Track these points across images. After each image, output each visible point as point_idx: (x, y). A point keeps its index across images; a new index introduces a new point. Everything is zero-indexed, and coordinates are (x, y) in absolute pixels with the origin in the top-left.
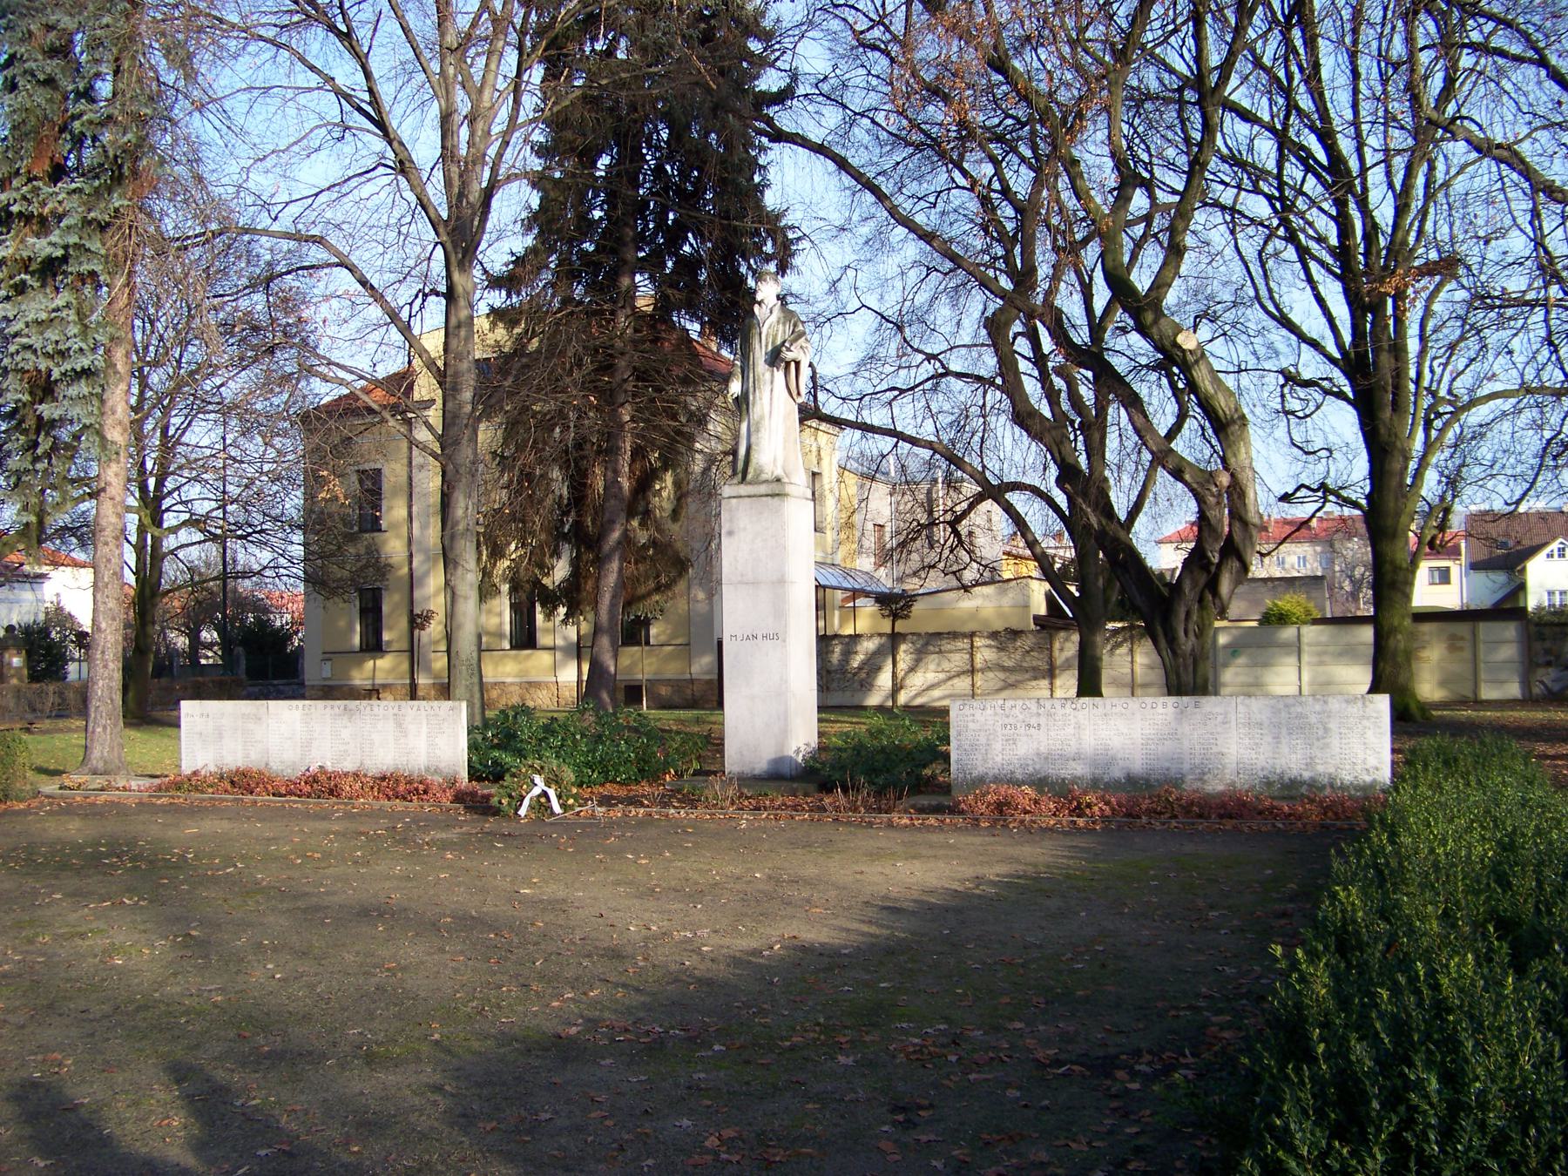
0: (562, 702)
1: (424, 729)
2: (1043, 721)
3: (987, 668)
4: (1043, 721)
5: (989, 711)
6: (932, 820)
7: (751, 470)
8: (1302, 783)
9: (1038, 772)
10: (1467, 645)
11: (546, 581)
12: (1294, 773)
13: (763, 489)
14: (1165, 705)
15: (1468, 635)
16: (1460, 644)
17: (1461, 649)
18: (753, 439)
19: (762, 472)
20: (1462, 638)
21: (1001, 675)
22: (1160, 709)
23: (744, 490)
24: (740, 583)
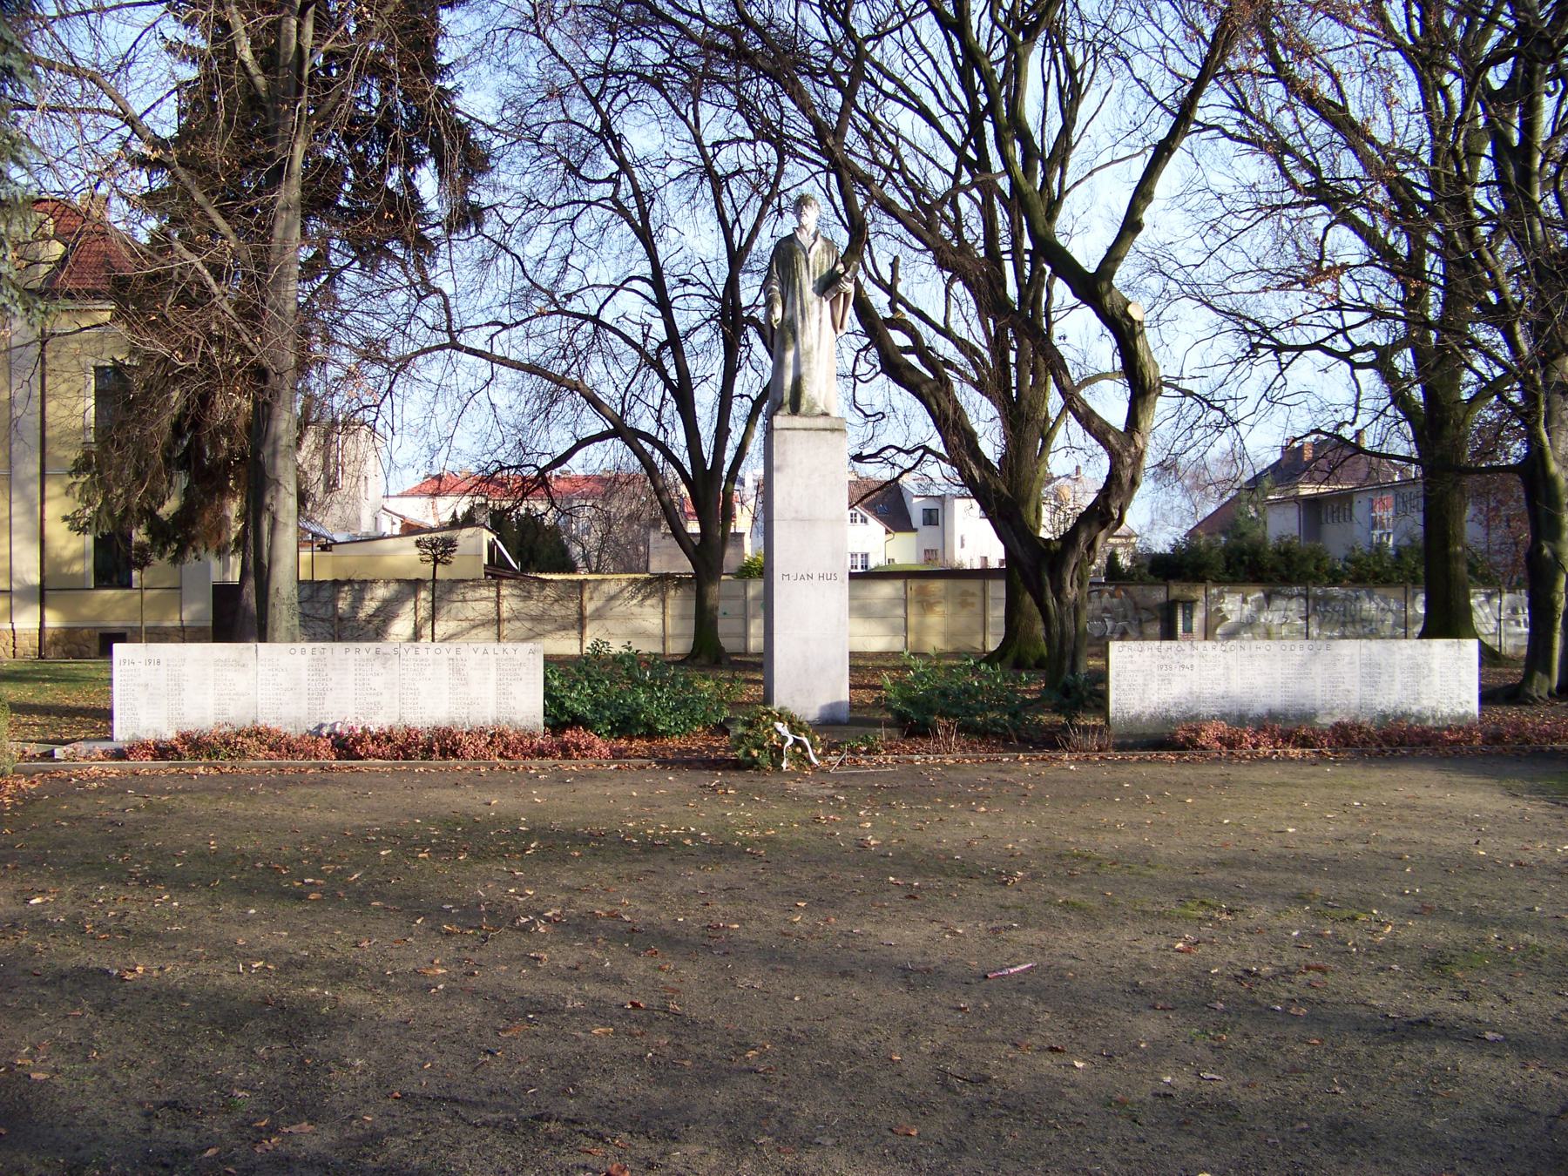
0: (19, 651)
1: (493, 675)
2: (1195, 662)
3: (517, 617)
4: (1195, 662)
5: (1147, 653)
6: (1295, 752)
7: (803, 401)
8: (1412, 715)
9: (1190, 709)
10: (977, 601)
11: (161, 512)
12: (1404, 707)
13: (821, 422)
14: (1302, 648)
15: (979, 593)
16: (970, 600)
17: (972, 604)
18: (803, 369)
19: (815, 404)
20: (973, 595)
21: (528, 625)
22: (1298, 651)
23: (797, 421)
24: (795, 519)
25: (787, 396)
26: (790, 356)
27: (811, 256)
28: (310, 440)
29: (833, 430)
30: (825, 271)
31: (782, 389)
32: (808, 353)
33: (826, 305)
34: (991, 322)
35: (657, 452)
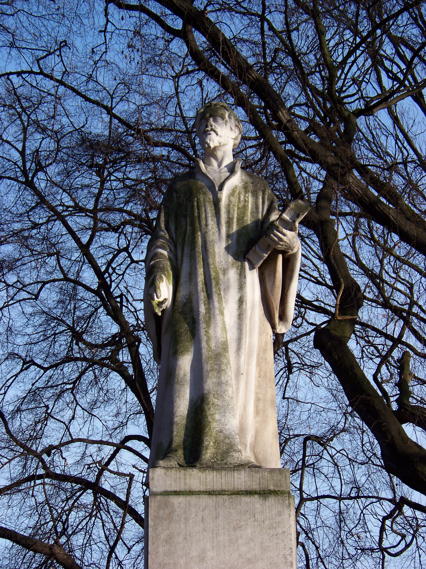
18: (210, 384)
23: (195, 479)
25: (179, 434)
26: (185, 363)
27: (224, 195)
28: (412, 258)
29: (264, 494)
30: (249, 220)
31: (171, 423)
32: (219, 355)
33: (252, 277)
34: (335, 291)
35: (150, 388)
